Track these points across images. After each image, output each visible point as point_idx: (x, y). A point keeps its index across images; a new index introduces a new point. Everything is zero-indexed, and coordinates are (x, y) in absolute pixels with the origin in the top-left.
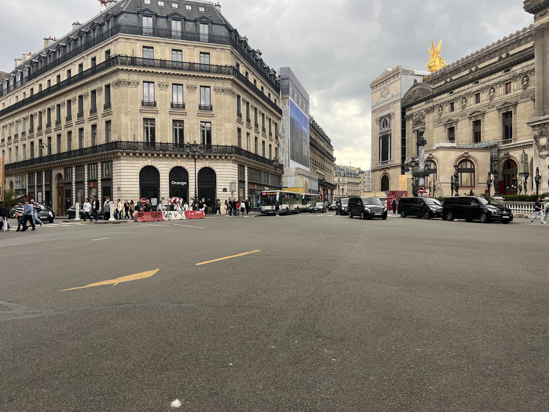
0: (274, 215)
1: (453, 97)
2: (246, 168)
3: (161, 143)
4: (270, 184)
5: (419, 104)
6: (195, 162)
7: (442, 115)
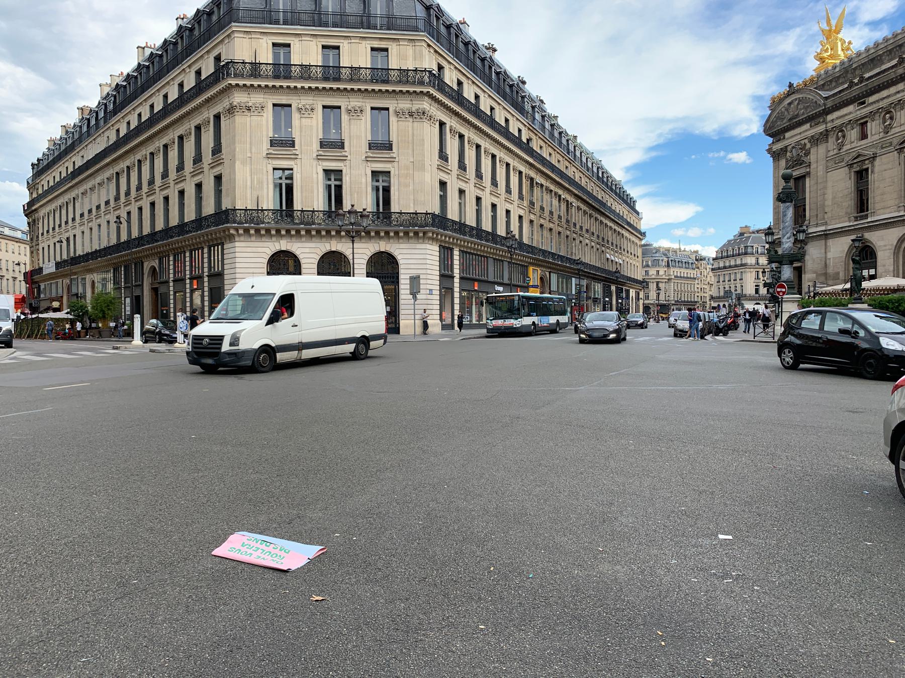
0: (734, 326)
1: (866, 111)
2: (456, 253)
3: (302, 211)
4: (506, 281)
5: (799, 129)
6: (353, 242)
7: (844, 147)
